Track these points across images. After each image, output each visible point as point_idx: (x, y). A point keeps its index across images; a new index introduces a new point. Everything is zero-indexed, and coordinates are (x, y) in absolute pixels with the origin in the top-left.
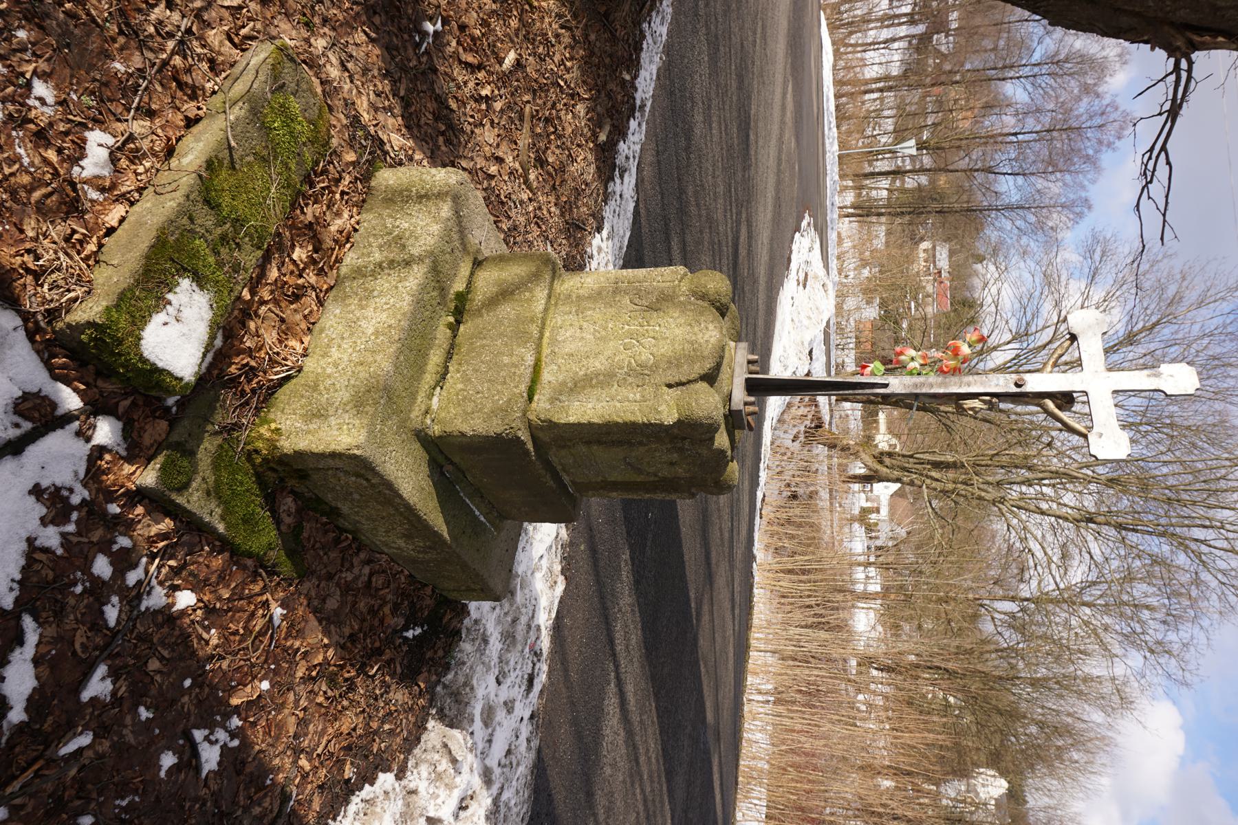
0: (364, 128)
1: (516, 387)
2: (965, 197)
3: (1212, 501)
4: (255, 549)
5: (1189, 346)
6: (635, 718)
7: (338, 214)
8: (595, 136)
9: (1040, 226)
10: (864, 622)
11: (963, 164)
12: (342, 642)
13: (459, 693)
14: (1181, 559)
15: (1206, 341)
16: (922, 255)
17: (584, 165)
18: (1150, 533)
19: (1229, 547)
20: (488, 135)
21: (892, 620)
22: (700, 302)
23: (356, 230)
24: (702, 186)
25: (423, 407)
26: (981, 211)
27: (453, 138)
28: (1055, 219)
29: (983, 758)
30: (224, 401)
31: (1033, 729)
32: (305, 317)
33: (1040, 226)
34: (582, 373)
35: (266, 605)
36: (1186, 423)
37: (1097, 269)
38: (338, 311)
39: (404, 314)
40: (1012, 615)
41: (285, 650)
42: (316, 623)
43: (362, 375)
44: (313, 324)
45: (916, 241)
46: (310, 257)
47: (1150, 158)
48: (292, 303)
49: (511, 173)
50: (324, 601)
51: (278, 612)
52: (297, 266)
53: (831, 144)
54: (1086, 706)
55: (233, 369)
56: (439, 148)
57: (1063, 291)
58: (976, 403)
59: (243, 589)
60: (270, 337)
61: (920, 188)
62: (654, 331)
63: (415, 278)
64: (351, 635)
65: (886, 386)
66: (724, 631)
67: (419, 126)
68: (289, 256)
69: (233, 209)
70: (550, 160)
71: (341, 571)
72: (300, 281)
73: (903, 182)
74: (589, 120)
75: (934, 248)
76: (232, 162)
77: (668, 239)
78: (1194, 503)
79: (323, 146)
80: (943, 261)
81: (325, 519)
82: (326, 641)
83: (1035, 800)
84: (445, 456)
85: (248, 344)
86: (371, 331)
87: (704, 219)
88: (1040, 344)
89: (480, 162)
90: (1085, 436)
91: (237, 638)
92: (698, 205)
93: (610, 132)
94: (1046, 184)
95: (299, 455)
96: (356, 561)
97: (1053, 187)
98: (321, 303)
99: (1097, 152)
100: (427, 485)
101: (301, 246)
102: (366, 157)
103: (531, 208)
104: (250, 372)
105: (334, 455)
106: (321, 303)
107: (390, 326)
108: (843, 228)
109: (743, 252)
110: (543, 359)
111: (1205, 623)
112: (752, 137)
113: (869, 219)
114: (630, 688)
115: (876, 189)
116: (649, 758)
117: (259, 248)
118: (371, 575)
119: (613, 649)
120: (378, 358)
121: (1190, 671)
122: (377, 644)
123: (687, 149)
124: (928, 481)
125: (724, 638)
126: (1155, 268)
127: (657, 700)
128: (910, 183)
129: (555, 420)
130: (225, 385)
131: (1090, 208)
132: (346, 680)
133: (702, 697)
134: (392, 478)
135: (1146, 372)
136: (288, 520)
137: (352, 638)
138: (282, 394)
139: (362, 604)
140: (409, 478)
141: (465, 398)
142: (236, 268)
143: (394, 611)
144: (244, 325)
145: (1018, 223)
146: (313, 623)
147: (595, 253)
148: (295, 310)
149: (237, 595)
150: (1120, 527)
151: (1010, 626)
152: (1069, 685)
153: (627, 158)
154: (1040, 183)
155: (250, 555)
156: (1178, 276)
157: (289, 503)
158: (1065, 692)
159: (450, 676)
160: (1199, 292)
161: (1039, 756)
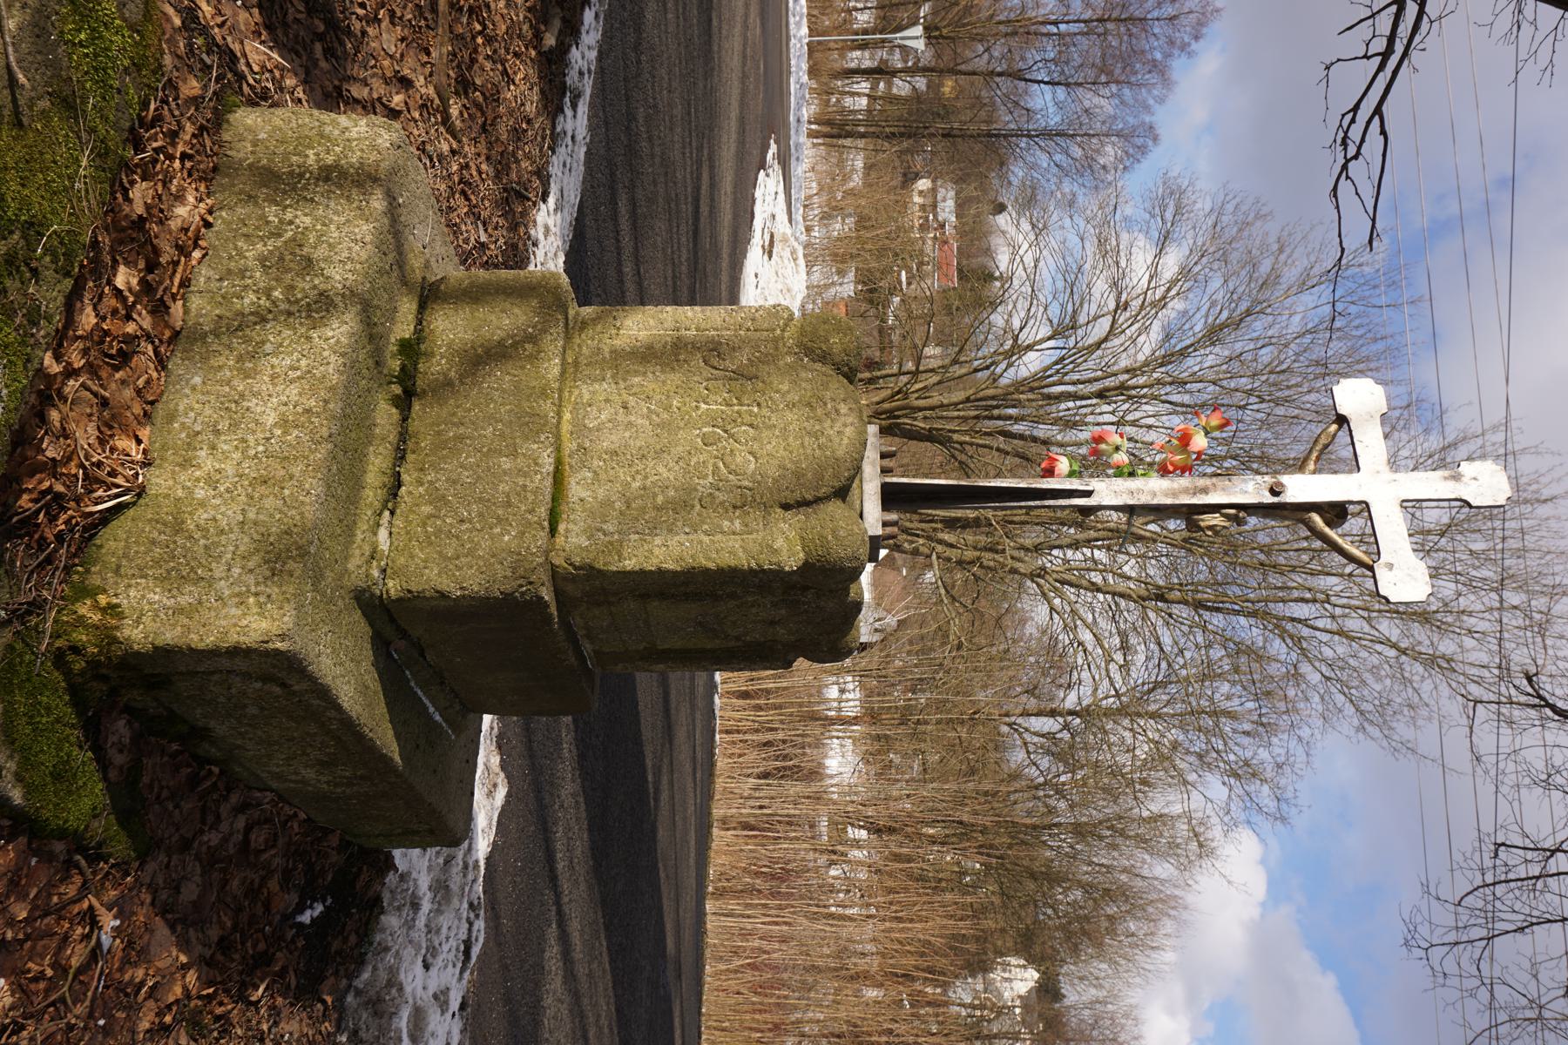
0: (205, 31)
1: (531, 511)
2: (983, 113)
3: (1315, 566)
4: (72, 823)
5: (1286, 346)
6: (581, 970)
7: (179, 198)
8: (538, 36)
9: (1088, 165)
10: (840, 761)
11: (981, 63)
12: (208, 953)
13: (380, 1000)
14: (1278, 647)
15: (1307, 339)
16: (917, 199)
17: (523, 92)
18: (1237, 613)
19: (1335, 627)
20: (386, 39)
21: (877, 751)
22: (818, 366)
23: (208, 225)
24: (655, 106)
25: (367, 549)
26: (1005, 136)
27: (336, 45)
28: (1110, 153)
29: (1010, 944)
30: (12, 562)
31: (1077, 894)
32: (139, 392)
33: (1088, 165)
34: (636, 485)
35: (91, 919)
36: (1281, 455)
37: (1168, 232)
38: (197, 380)
39: (332, 389)
40: (1049, 736)
41: (121, 988)
42: (166, 931)
43: (269, 503)
44: (152, 403)
45: (909, 178)
46: (142, 281)
47: (1353, 121)
48: (116, 369)
49: (423, 106)
50: (177, 890)
51: (109, 922)
52: (125, 299)
53: (798, 24)
54: (1147, 857)
55: (24, 501)
56: (315, 63)
57: (1123, 264)
58: (1215, 520)
59: (50, 896)
60: (86, 434)
61: (917, 96)
62: (751, 413)
63: (340, 330)
64: (222, 939)
65: (1088, 494)
66: (686, 810)
67: (285, 25)
68: (109, 282)
69: (25, 203)
70: (478, 82)
71: (202, 832)
72: (131, 328)
73: (889, 85)
74: (529, 10)
75: (934, 190)
76: (17, 112)
77: (613, 201)
78: (1293, 569)
79: (154, 72)
80: (947, 209)
81: (175, 747)
82: (183, 959)
83: (1075, 994)
84: (404, 631)
85: (50, 453)
86: (271, 419)
87: (657, 160)
88: (1090, 341)
89: (379, 88)
90: (1371, 569)
91: (42, 985)
92: (650, 139)
93: (560, 31)
94: (1096, 100)
95: (165, 653)
96: (224, 810)
97: (1101, 103)
98: (161, 364)
99: (1167, 56)
100: (372, 679)
101: (127, 263)
102: (213, 87)
103: (455, 168)
104: (55, 503)
105: (236, 652)
106: (161, 364)
107: (308, 411)
108: (807, 153)
109: (704, 209)
110: (567, 460)
111: (1305, 732)
112: (715, 23)
113: (840, 142)
114: (574, 926)
115: (853, 94)
116: (601, 1029)
117: (68, 274)
118: (248, 829)
119: (552, 870)
120: (296, 470)
121: (1286, 801)
122: (262, 946)
123: (636, 47)
124: (939, 548)
125: (685, 819)
126: (1246, 233)
127: (608, 938)
128: (901, 87)
129: (600, 565)
130: (12, 534)
131: (1155, 139)
132: (218, 1018)
133: (662, 917)
134: (328, 680)
135: (1440, 473)
136: (119, 759)
137: (224, 945)
138: (112, 540)
139: (235, 883)
140: (346, 673)
141: (439, 531)
142: (34, 317)
143: (285, 885)
144: (43, 419)
145: (1057, 157)
146: (162, 930)
147: (541, 237)
148: (123, 382)
149: (40, 910)
150: (1199, 605)
151: (1048, 752)
152: (1118, 829)
153: (581, 73)
154: (1089, 99)
155: (62, 834)
156: (1275, 247)
157: (121, 729)
158: (1119, 840)
159: (366, 975)
160: (1299, 269)
161: (1085, 933)
